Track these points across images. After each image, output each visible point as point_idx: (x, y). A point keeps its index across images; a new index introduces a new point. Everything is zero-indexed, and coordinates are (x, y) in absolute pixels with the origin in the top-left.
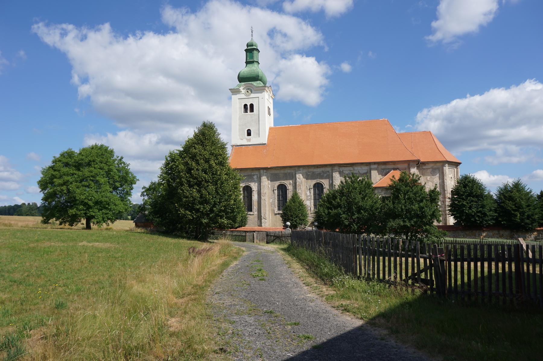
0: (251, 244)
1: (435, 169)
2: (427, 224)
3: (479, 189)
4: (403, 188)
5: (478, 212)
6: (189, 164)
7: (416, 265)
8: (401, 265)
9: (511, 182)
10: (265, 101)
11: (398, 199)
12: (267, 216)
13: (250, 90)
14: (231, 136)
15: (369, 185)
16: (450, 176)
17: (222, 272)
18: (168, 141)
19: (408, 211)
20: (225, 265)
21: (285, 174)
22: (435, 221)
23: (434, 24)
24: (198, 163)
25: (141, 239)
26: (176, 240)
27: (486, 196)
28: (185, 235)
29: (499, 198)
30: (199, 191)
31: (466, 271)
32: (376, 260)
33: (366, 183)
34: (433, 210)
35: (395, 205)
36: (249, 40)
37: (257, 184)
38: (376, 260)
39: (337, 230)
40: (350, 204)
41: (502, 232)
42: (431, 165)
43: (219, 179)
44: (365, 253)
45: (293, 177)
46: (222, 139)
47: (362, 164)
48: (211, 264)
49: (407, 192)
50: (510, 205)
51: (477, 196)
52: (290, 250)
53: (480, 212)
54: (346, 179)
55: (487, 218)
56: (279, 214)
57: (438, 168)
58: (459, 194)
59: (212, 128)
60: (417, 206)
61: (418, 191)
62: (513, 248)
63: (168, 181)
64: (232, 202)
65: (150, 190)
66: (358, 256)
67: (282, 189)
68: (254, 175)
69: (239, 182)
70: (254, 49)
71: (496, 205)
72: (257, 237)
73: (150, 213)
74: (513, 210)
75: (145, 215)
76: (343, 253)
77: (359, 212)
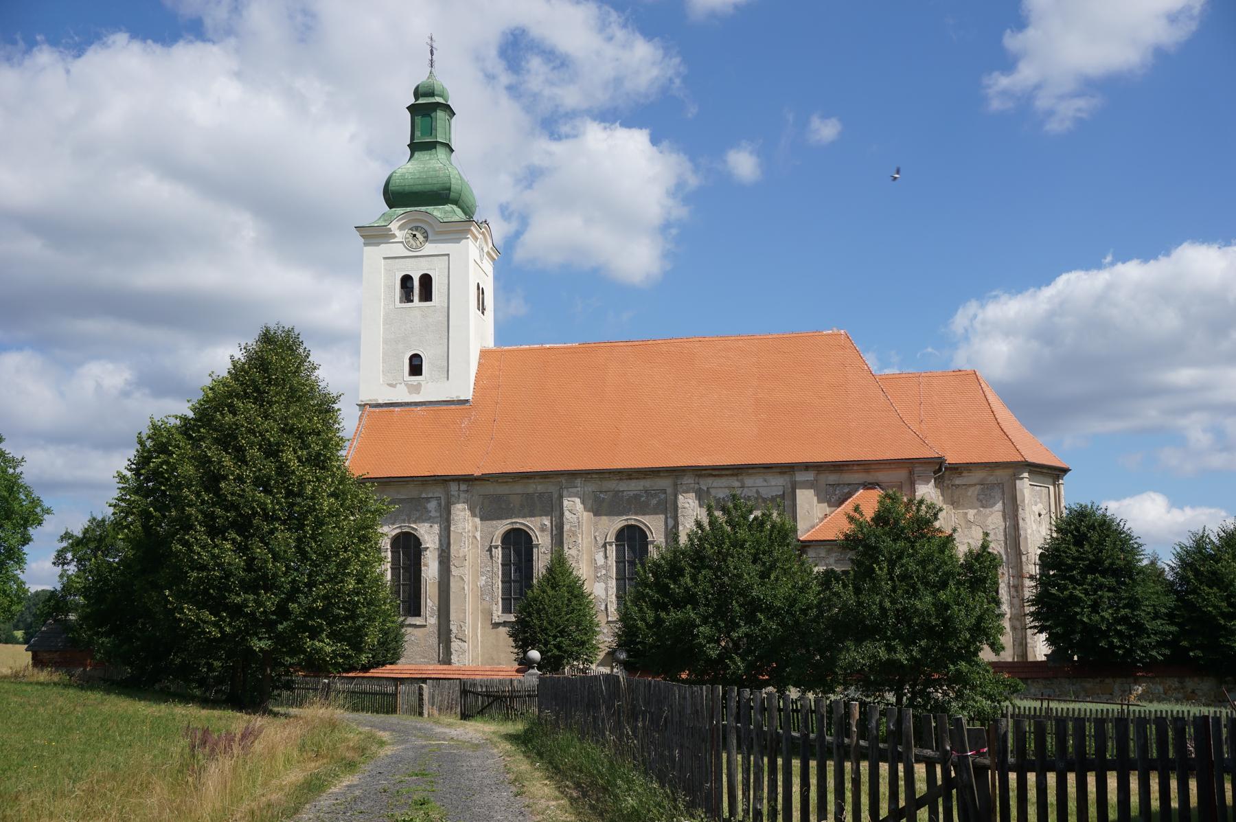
0: (411, 721)
1: (992, 487)
2: (962, 658)
3: (1122, 550)
4: (887, 543)
5: (1118, 621)
6: (210, 462)
7: (902, 783)
8: (856, 782)
9: (1216, 529)
10: (467, 266)
11: (872, 579)
12: (468, 631)
13: (422, 232)
14: (355, 375)
15: (784, 534)
16: (1036, 509)
17: (297, 810)
18: (160, 385)
19: (904, 615)
20: (313, 787)
21: (529, 496)
22: (986, 647)
23: (1012, 41)
24: (240, 455)
25: (44, 705)
26: (163, 706)
27: (1141, 571)
28: (197, 692)
29: (1183, 579)
30: (242, 549)
31: (1052, 798)
32: (901, 774)
33: (773, 527)
34: (978, 612)
35: (862, 598)
36: (421, 78)
37: (436, 527)
38: (901, 774)
39: (684, 676)
40: (722, 599)
41: (1190, 684)
42: (978, 475)
43: (312, 509)
44: (746, 745)
45: (553, 508)
46: (322, 384)
48: (265, 784)
49: (900, 557)
50: (1213, 600)
51: (1115, 572)
52: (530, 741)
53: (1124, 620)
54: (710, 514)
55: (1144, 641)
56: (505, 624)
57: (1000, 485)
58: (1062, 563)
59: (290, 348)
60: (929, 599)
61: (932, 554)
62: (1190, 731)
63: (145, 515)
64: (351, 584)
65: (87, 544)
66: (725, 756)
67: (518, 546)
68: (428, 500)
69: (374, 520)
70: (438, 104)
71: (1170, 601)
72: (432, 697)
73: (84, 618)
74: (1223, 615)
75: (67, 627)
76: (681, 747)
77: (751, 619)
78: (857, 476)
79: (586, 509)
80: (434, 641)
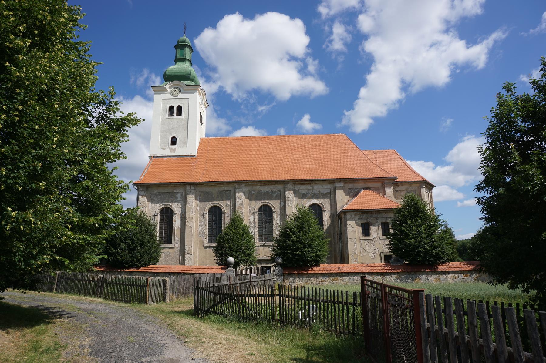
12: (193, 250)
21: (221, 192)
37: (180, 205)
47: (324, 181)
56: (210, 247)
67: (216, 213)
68: (177, 193)
72: (172, 288)
78: (360, 185)
79: (246, 198)
80: (177, 254)
